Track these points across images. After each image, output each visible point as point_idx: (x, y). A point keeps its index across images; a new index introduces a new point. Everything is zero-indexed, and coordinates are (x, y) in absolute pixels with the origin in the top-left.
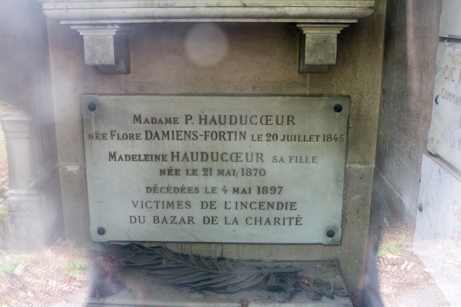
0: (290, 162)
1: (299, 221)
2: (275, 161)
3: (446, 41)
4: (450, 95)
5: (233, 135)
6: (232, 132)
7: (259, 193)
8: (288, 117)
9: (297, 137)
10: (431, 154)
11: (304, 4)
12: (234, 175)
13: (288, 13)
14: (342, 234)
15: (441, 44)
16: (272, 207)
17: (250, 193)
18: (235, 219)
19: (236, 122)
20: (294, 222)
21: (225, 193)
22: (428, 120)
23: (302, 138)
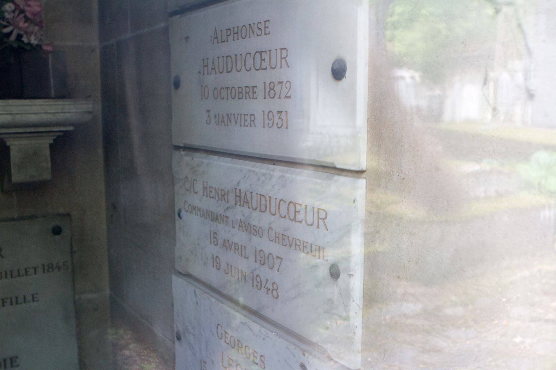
0: (3, 305)
3: (182, 150)
10: (180, 273)
15: (177, 155)
22: (172, 237)
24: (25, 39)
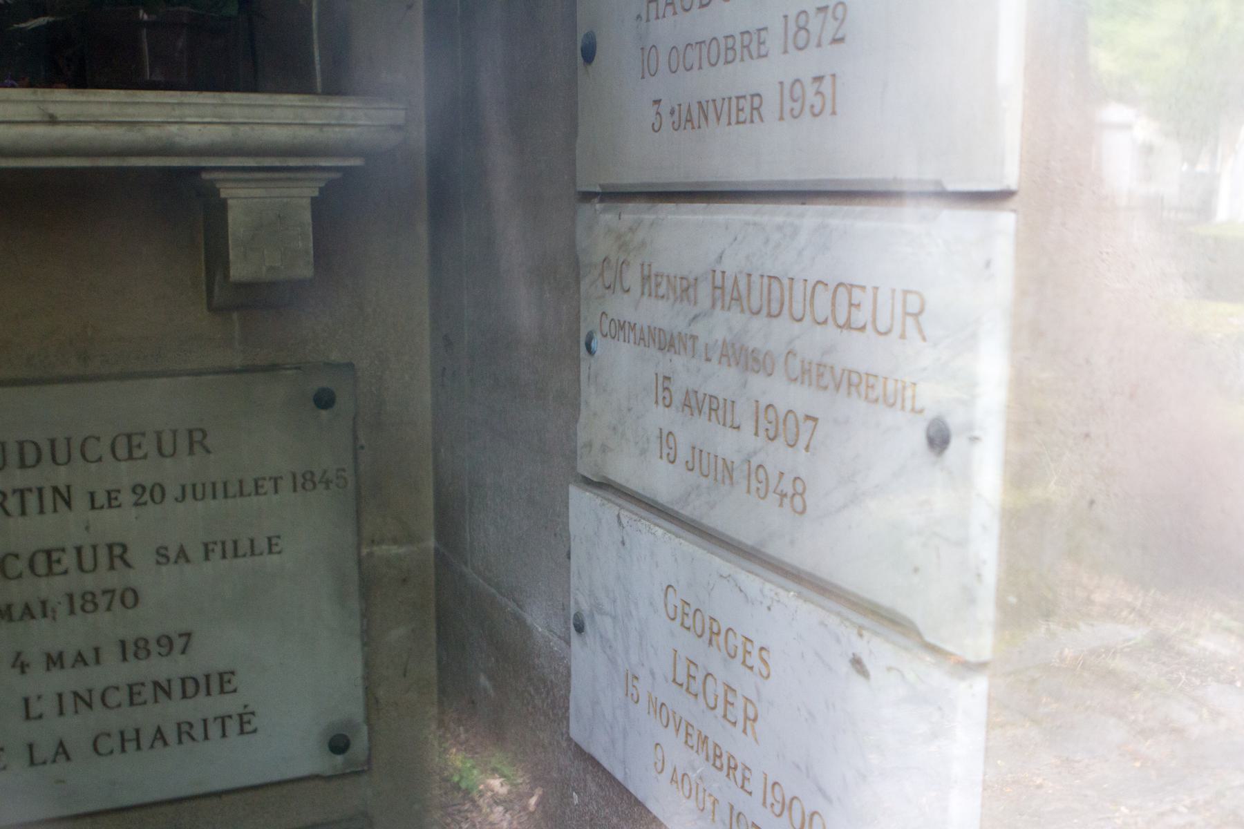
0: (207, 558)
1: (249, 722)
2: (163, 560)
3: (596, 200)
4: (622, 328)
5: (32, 500)
6: (30, 490)
7: (125, 659)
8: (190, 432)
9: (220, 487)
11: (221, 117)
12: (45, 615)
13: (177, 139)
14: (370, 739)
16: (168, 694)
17: (98, 662)
18: (61, 744)
19: (39, 460)
20: (233, 726)
21: (23, 672)
22: (571, 402)
23: (233, 489)
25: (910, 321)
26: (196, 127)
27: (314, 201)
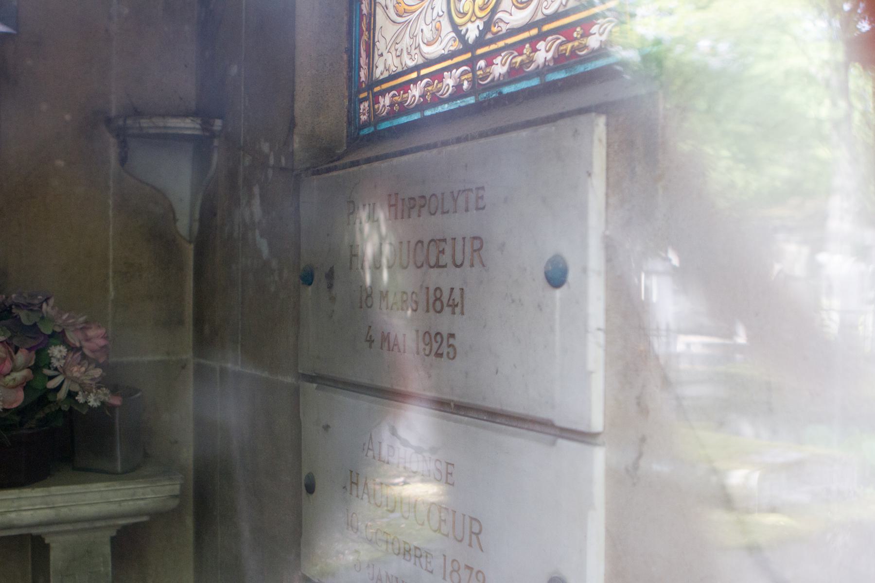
24: (80, 398)
25: (474, 537)
26: (29, 513)
27: (113, 540)
